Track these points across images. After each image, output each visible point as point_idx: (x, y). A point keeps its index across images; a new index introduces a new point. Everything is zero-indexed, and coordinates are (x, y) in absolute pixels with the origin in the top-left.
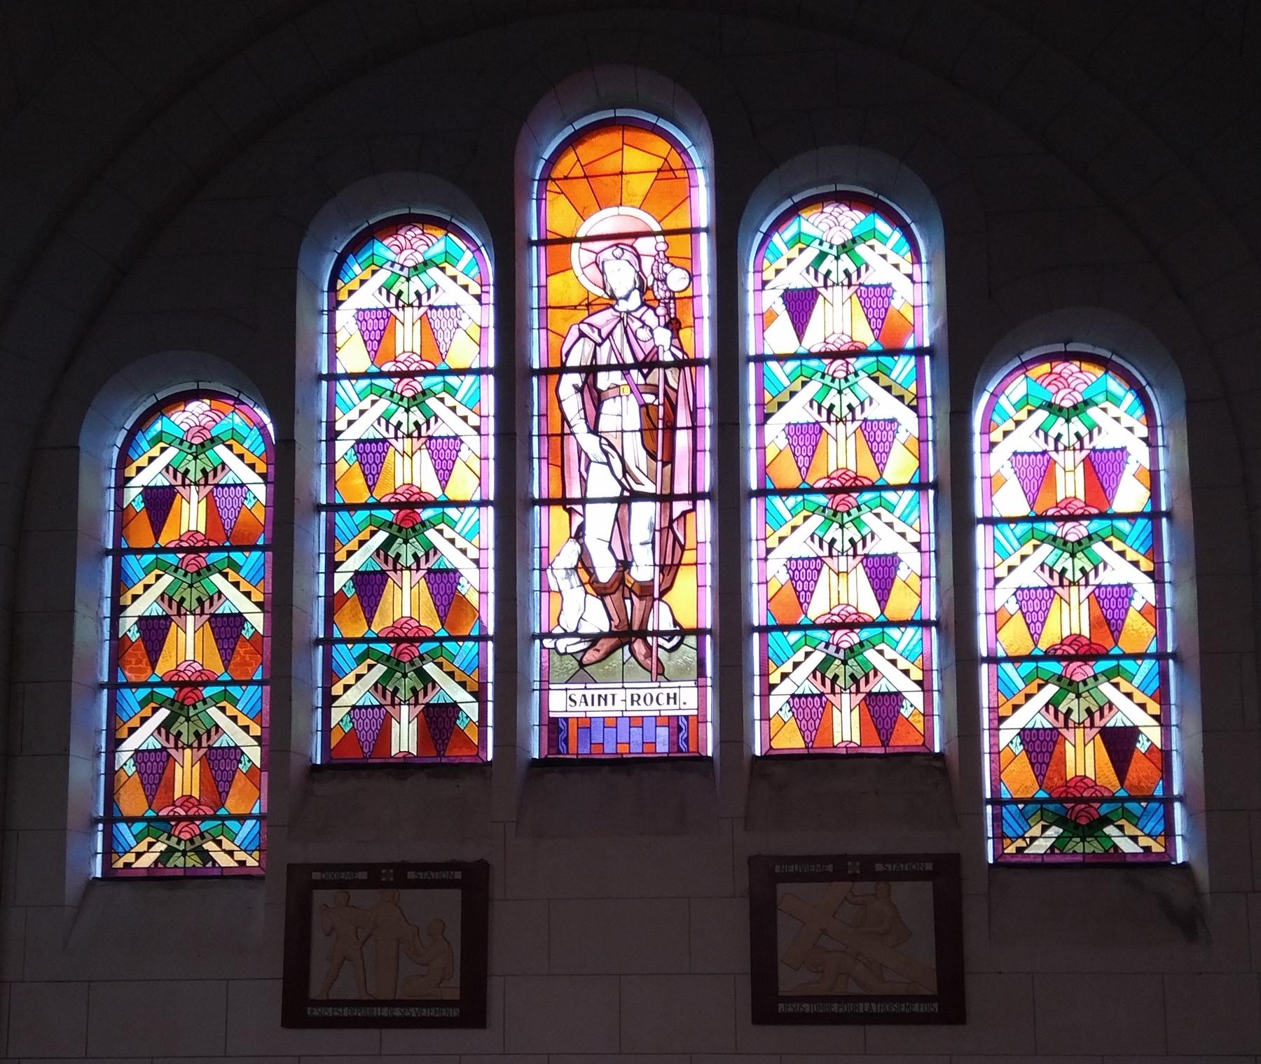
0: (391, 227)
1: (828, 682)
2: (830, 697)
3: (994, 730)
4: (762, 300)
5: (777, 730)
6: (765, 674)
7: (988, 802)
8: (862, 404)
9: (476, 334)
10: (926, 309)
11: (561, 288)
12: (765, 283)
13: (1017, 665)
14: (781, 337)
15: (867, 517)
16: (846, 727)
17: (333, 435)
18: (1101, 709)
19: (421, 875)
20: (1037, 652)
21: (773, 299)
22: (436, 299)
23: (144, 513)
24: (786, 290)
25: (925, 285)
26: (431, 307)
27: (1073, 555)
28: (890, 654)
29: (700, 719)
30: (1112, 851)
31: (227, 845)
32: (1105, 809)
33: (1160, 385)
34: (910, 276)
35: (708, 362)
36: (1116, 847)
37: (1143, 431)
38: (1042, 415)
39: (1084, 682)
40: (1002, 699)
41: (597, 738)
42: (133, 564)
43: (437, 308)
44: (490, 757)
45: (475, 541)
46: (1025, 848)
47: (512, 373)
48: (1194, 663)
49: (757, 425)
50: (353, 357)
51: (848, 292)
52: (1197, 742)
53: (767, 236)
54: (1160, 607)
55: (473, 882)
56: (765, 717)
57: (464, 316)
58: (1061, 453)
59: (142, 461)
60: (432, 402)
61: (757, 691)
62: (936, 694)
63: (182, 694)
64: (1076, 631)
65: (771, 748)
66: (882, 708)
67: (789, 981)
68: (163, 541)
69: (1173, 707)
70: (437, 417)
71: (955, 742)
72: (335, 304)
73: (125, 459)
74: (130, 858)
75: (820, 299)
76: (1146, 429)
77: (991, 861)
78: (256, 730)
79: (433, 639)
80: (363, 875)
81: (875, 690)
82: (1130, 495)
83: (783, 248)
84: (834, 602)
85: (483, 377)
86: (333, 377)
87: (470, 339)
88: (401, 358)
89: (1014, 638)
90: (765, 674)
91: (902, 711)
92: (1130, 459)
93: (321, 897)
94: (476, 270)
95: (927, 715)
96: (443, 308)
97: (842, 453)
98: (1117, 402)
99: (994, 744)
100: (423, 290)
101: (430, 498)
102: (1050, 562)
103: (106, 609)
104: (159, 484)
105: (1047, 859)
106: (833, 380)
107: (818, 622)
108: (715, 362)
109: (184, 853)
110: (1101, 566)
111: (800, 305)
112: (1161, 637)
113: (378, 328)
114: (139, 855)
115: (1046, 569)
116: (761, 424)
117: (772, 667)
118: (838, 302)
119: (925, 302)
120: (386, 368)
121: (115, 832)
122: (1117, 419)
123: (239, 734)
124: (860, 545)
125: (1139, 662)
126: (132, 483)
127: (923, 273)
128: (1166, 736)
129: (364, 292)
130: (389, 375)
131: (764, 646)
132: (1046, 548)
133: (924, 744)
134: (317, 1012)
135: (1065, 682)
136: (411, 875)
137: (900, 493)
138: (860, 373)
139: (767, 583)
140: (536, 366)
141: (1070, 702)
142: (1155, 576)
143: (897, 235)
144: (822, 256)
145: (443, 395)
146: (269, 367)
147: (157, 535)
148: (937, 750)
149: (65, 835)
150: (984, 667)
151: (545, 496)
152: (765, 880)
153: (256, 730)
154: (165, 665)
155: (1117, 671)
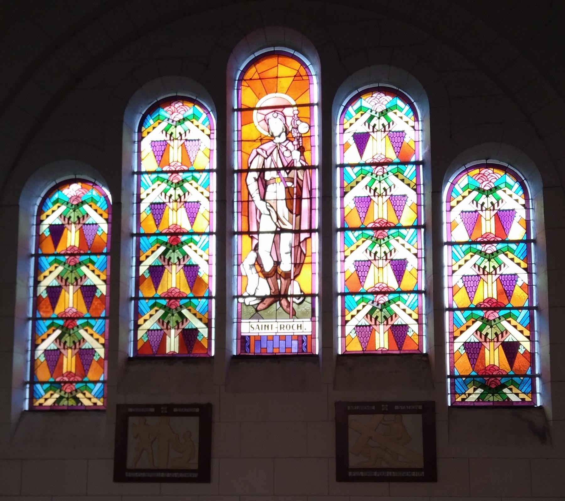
0: (168, 102)
1: (373, 320)
2: (374, 327)
3: (452, 343)
4: (343, 138)
5: (349, 341)
6: (343, 316)
7: (449, 377)
8: (390, 187)
10: (421, 143)
11: (248, 132)
12: (344, 130)
13: (462, 312)
14: (352, 155)
15: (392, 241)
16: (382, 341)
17: (139, 201)
18: (502, 333)
19: (180, 410)
20: (472, 306)
21: (348, 138)
22: (189, 137)
23: (45, 362)
24: (355, 133)
25: (420, 131)
26: (186, 140)
27: (489, 260)
28: (403, 306)
29: (313, 337)
30: (506, 400)
31: (88, 395)
32: (503, 380)
33: (531, 180)
34: (413, 127)
36: (508, 398)
37: (523, 202)
38: (475, 193)
39: (494, 320)
40: (455, 328)
41: (264, 346)
42: (44, 261)
43: (189, 141)
44: (213, 354)
46: (465, 399)
47: (225, 172)
48: (546, 312)
49: (342, 326)
51: (384, 135)
52: (547, 348)
53: (346, 107)
54: (530, 285)
55: (205, 414)
56: (343, 336)
57: (201, 144)
58: (484, 212)
59: (49, 212)
61: (340, 323)
63: (69, 260)
64: (490, 296)
65: (346, 351)
66: (398, 332)
67: (354, 461)
68: (59, 250)
71: (433, 348)
72: (141, 138)
73: (40, 211)
74: (41, 401)
75: (371, 138)
76: (524, 201)
77: (449, 405)
78: (104, 277)
79: (186, 298)
82: (517, 232)
84: (377, 282)
87: (205, 154)
88: (172, 164)
89: (461, 299)
90: (343, 316)
91: (408, 333)
94: (208, 123)
95: (420, 335)
96: (192, 140)
97: (381, 211)
98: (511, 188)
99: (451, 349)
101: (185, 231)
102: (478, 263)
105: (476, 404)
107: (369, 291)
108: (321, 167)
109: (68, 399)
110: (502, 265)
111: (361, 140)
112: (530, 299)
113: (161, 149)
114: (46, 399)
116: (342, 197)
117: (347, 312)
119: (420, 140)
120: (164, 169)
121: (35, 388)
123: (93, 341)
125: (520, 311)
127: (419, 126)
129: (155, 133)
131: (342, 174)
132: (477, 257)
133: (418, 349)
135: (485, 320)
136: (175, 410)
137: (408, 230)
138: (390, 236)
139: (345, 337)
141: (487, 330)
142: (528, 270)
144: (372, 117)
146: (110, 168)
148: (424, 352)
150: (447, 313)
152: (343, 412)
153: (106, 215)
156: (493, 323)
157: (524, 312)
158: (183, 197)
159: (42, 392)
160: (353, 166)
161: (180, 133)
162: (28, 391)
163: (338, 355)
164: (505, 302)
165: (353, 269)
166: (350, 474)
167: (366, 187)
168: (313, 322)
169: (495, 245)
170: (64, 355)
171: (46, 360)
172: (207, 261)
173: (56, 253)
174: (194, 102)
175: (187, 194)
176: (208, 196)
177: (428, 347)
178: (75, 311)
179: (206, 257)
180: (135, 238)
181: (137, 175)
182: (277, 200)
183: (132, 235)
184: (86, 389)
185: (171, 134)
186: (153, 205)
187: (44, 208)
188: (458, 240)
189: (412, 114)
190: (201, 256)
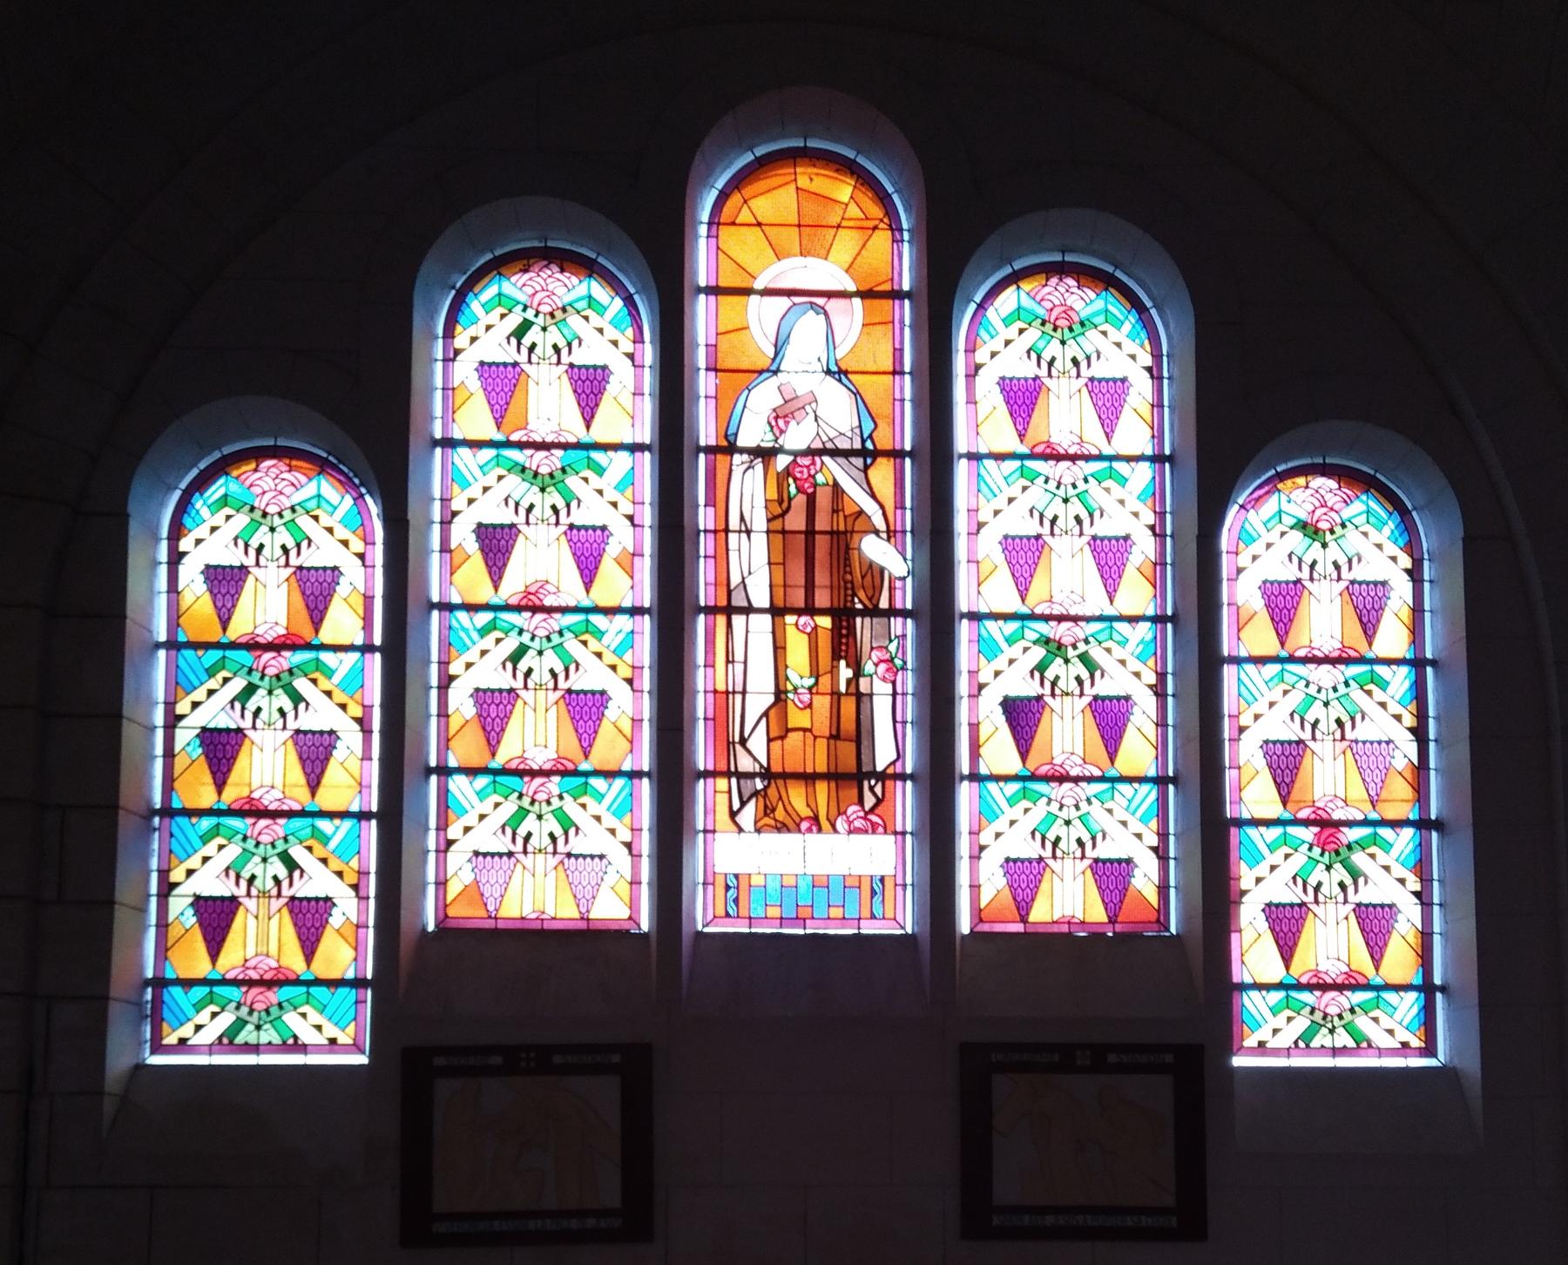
0: (523, 260)
9: (627, 727)
17: (447, 681)
22: (577, 845)
26: (569, 855)
31: (325, 520)
33: (1427, 507)
35: (908, 295)
40: (1243, 705)
45: (629, 493)
47: (672, 445)
50: (475, 420)
52: (1468, 928)
59: (202, 532)
60: (574, 321)
62: (1168, 540)
66: (1111, 876)
67: (1007, 1188)
69: (1432, 773)
70: (577, 829)
71: (1199, 921)
80: (496, 1060)
81: (1103, 856)
83: (999, 325)
85: (638, 454)
86: (444, 771)
87: (628, 413)
92: (1392, 594)
93: (445, 1088)
95: (1163, 889)
100: (562, 344)
103: (159, 718)
104: (222, 725)
106: (1055, 329)
113: (502, 383)
114: (198, 1028)
115: (1295, 559)
118: (1068, 876)
120: (515, 437)
122: (1387, 868)
123: (335, 873)
124: (1089, 845)
126: (183, 723)
128: (1427, 918)
130: (521, 445)
134: (441, 1228)
136: (557, 1059)
140: (702, 283)
143: (1133, 317)
145: (588, 312)
147: (214, 954)
149: (117, 815)
151: (712, 603)
154: (231, 958)
155: (1375, 840)
156: (1328, 537)
157: (1408, 832)
158: (561, 841)
159: (190, 1011)
160: (1000, 457)
161: (552, 671)
162: (148, 1029)
163: (963, 937)
164: (1369, 969)
165: (1001, 881)
166: (996, 1221)
167: (1033, 833)
168: (896, 241)
169: (1342, 667)
170: (251, 954)
171: (201, 922)
172: (631, 518)
173: (224, 640)
174: (588, 268)
175: (574, 504)
176: (628, 839)
177: (1185, 918)
178: (283, 632)
179: (626, 507)
180: (434, 779)
181: (439, 775)
182: (799, 226)
183: (429, 771)
184: (317, 669)
185: (529, 672)
186: (482, 696)
187: (187, 521)
188: (1258, 815)
189: (1143, 335)
190: (615, 505)
